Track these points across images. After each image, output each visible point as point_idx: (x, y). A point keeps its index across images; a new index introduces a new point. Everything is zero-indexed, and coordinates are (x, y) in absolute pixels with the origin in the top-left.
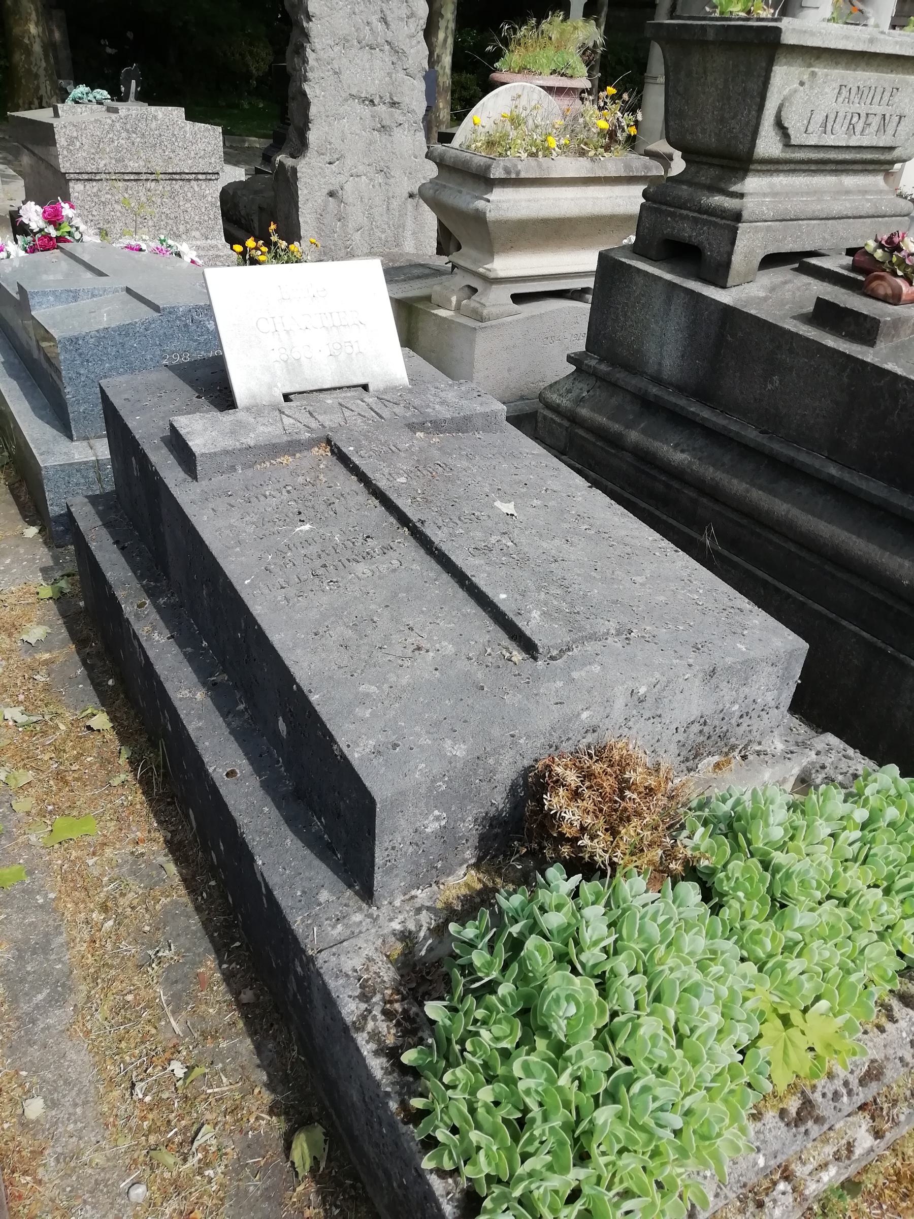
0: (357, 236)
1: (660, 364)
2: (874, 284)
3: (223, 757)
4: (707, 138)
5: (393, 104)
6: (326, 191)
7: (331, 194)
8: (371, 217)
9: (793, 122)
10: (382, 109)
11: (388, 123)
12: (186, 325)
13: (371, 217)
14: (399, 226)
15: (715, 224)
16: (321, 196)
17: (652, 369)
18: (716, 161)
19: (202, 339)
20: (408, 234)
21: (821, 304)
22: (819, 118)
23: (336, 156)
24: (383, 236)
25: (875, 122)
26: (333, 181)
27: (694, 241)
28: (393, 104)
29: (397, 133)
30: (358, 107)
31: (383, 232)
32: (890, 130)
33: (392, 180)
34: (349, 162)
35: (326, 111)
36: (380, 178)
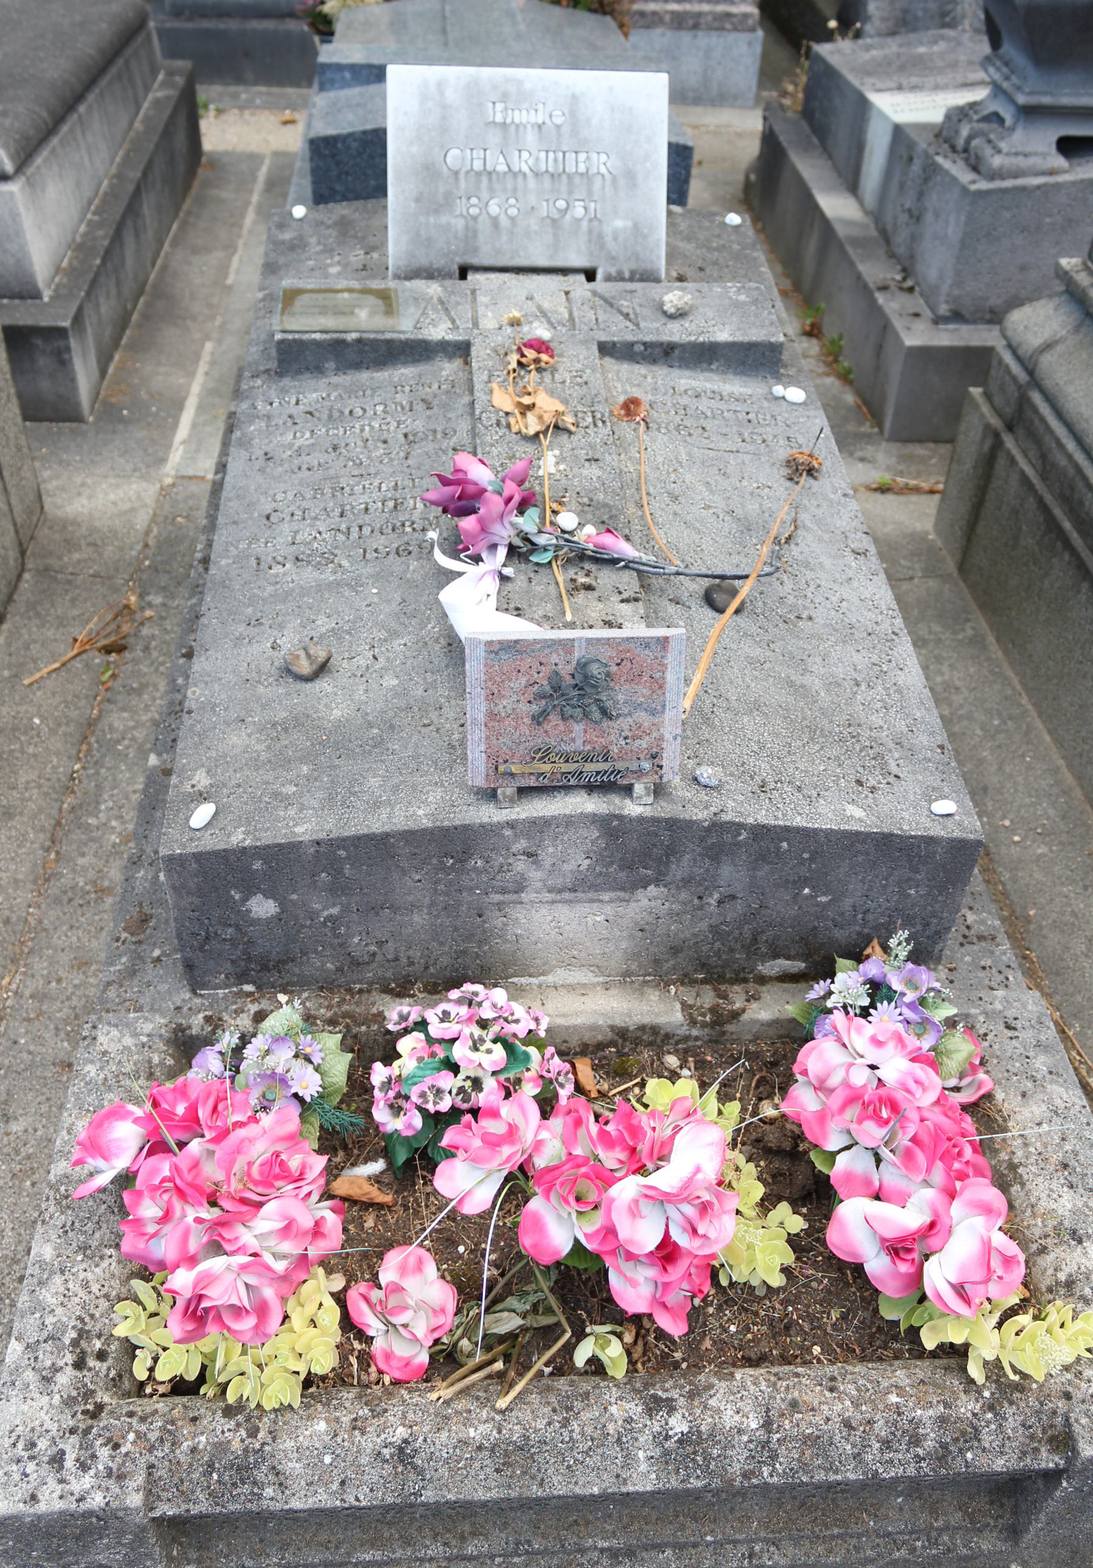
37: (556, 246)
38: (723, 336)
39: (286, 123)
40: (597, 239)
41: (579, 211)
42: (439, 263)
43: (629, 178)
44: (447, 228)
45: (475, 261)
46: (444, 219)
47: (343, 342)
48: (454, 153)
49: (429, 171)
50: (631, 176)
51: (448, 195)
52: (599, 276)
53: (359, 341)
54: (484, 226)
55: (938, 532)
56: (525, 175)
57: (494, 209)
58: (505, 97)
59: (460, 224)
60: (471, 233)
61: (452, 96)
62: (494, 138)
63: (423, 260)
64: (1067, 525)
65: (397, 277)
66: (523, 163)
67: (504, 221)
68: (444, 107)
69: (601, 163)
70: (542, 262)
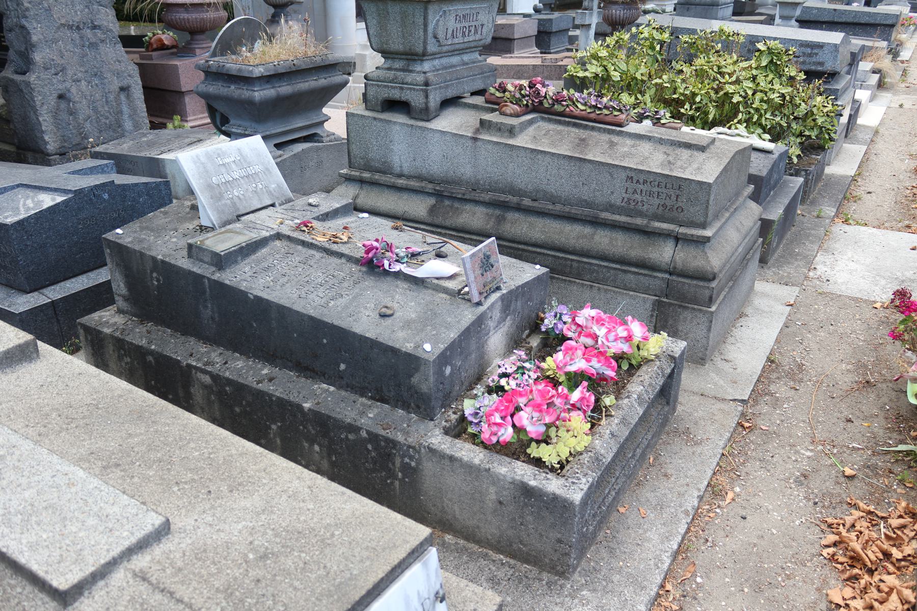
0: (87, 125)
1: (401, 167)
2: (504, 109)
3: (316, 396)
4: (397, 45)
5: (95, 27)
6: (55, 95)
7: (61, 97)
8: (95, 110)
9: (441, 36)
10: (88, 33)
11: (94, 40)
12: (91, 199)
13: (95, 110)
14: (118, 112)
15: (414, 89)
16: (52, 100)
17: (397, 170)
18: (403, 57)
19: (102, 207)
20: (126, 117)
21: (482, 122)
22: (450, 32)
23: (59, 69)
24: (108, 121)
25: (473, 29)
26: (60, 87)
27: (403, 99)
28: (95, 27)
29: (102, 47)
30: (68, 32)
31: (107, 118)
32: (479, 32)
33: (106, 80)
34: (70, 72)
35: (45, 38)
36: (96, 81)
37: (260, 200)
38: (337, 205)
39: (396, 228)
40: (270, 193)
41: (260, 186)
42: (230, 218)
43: (267, 170)
44: (226, 205)
45: (240, 213)
46: (223, 202)
47: (242, 247)
48: (214, 178)
49: (210, 187)
50: (267, 169)
51: (220, 193)
52: (277, 204)
53: (247, 245)
54: (236, 199)
55: (175, 162)
56: (24, 73)
57: (236, 194)
58: (219, 155)
59: (229, 202)
60: (234, 204)
61: (203, 159)
62: (223, 170)
63: (225, 219)
64: (585, 260)
65: (220, 227)
66: (236, 175)
67: (241, 197)
68: (203, 164)
69: (258, 168)
70: (260, 206)
